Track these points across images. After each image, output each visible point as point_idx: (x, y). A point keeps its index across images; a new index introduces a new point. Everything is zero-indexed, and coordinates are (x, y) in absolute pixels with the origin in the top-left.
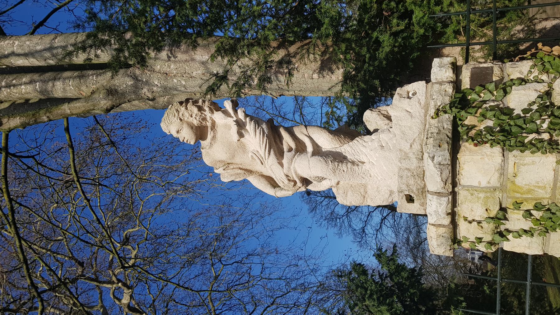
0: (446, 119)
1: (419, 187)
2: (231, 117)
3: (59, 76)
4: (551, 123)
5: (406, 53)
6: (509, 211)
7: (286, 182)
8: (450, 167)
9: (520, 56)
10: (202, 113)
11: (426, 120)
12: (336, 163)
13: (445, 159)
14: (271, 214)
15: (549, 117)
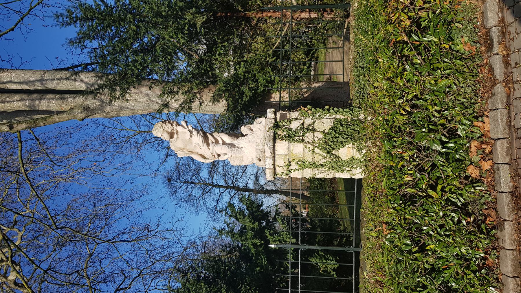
3: (44, 97)
5: (235, 17)
7: (211, 156)
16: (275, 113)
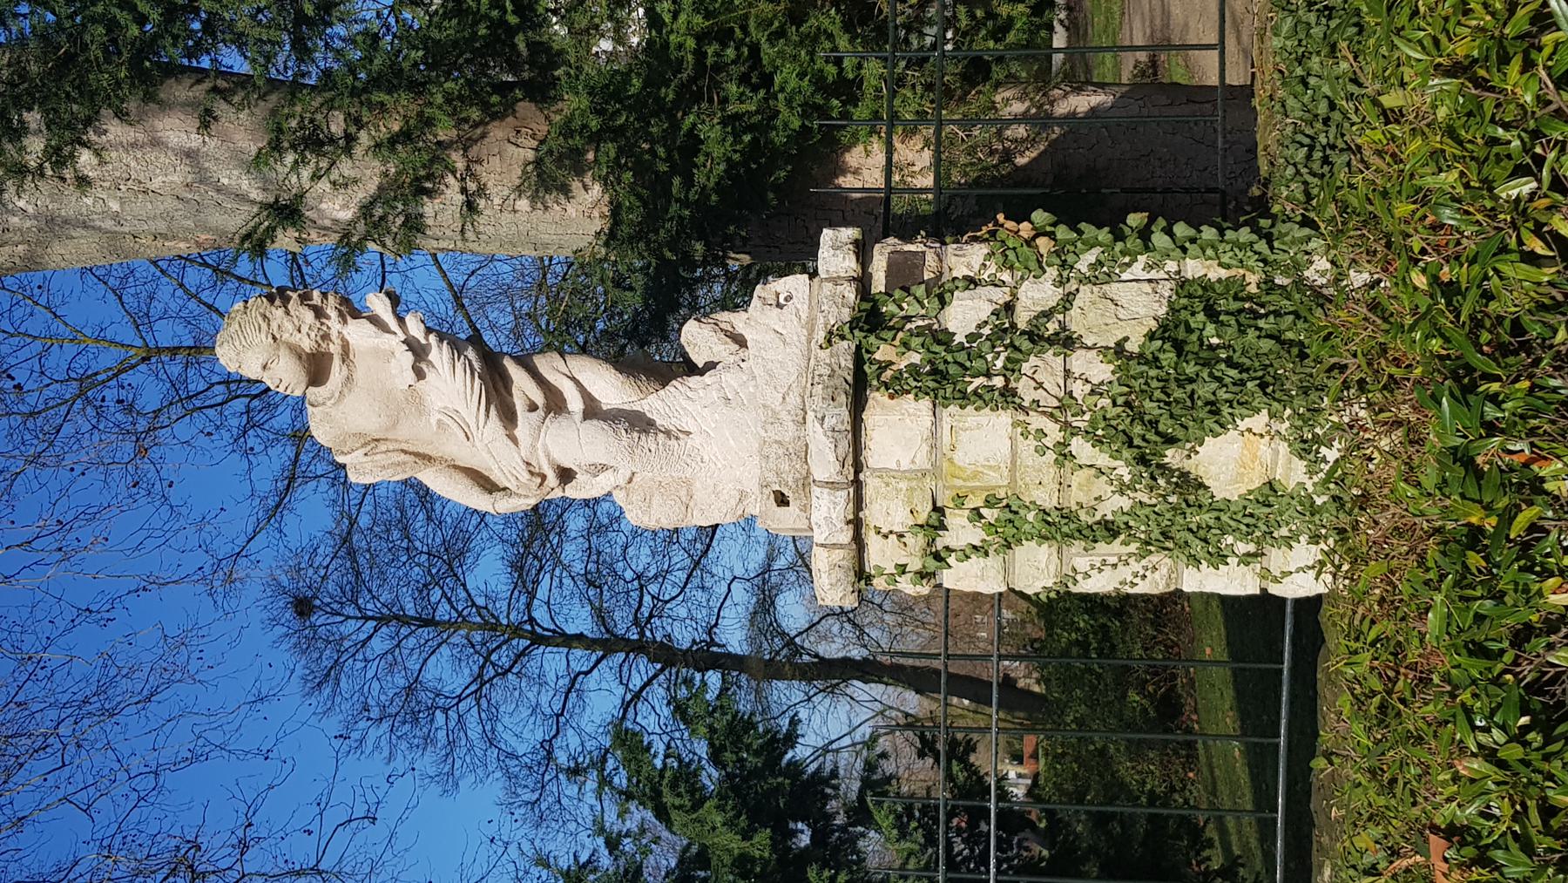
0: (844, 349)
1: (798, 475)
2: (388, 331)
4: (1008, 359)
5: (759, 164)
6: (947, 511)
8: (850, 436)
9: (970, 234)
10: (322, 324)
11: (809, 350)
12: (636, 435)
13: (842, 423)
14: (148, 699)
15: (1006, 348)
16: (862, 251)
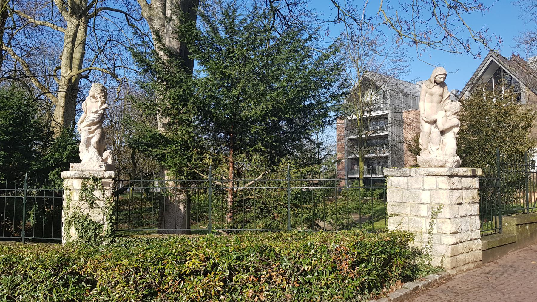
16: (110, 178)
